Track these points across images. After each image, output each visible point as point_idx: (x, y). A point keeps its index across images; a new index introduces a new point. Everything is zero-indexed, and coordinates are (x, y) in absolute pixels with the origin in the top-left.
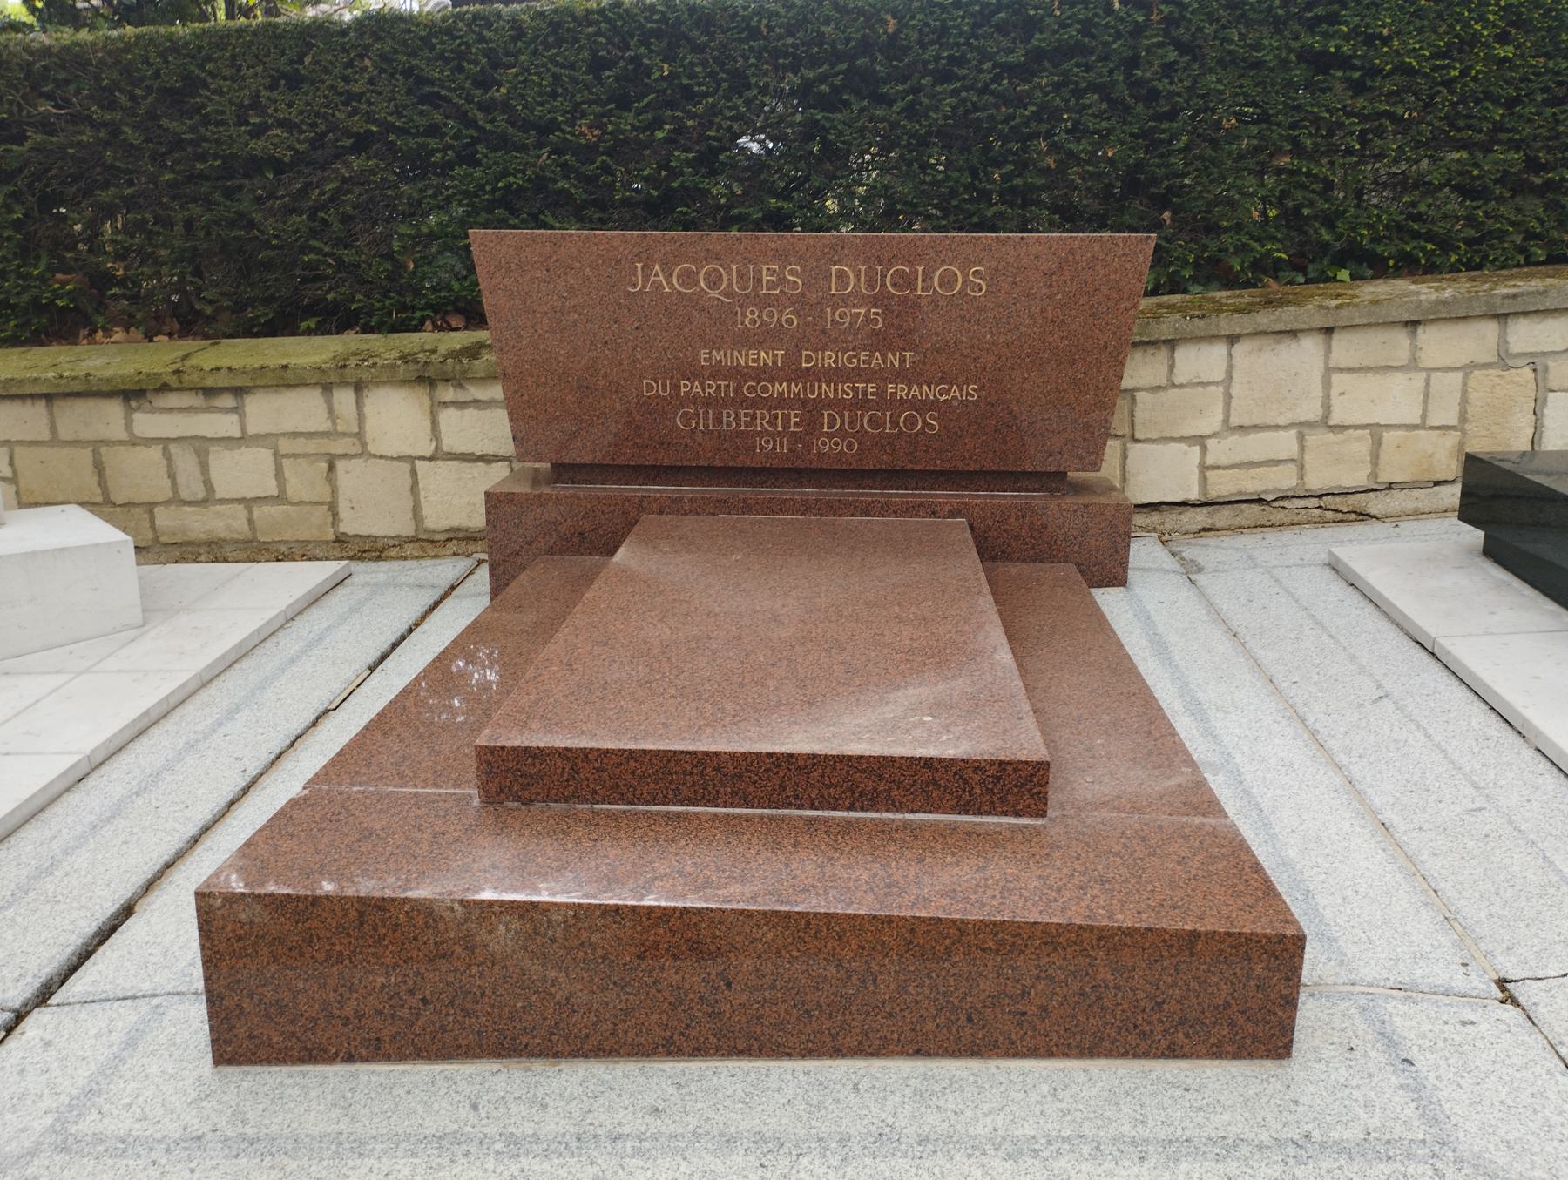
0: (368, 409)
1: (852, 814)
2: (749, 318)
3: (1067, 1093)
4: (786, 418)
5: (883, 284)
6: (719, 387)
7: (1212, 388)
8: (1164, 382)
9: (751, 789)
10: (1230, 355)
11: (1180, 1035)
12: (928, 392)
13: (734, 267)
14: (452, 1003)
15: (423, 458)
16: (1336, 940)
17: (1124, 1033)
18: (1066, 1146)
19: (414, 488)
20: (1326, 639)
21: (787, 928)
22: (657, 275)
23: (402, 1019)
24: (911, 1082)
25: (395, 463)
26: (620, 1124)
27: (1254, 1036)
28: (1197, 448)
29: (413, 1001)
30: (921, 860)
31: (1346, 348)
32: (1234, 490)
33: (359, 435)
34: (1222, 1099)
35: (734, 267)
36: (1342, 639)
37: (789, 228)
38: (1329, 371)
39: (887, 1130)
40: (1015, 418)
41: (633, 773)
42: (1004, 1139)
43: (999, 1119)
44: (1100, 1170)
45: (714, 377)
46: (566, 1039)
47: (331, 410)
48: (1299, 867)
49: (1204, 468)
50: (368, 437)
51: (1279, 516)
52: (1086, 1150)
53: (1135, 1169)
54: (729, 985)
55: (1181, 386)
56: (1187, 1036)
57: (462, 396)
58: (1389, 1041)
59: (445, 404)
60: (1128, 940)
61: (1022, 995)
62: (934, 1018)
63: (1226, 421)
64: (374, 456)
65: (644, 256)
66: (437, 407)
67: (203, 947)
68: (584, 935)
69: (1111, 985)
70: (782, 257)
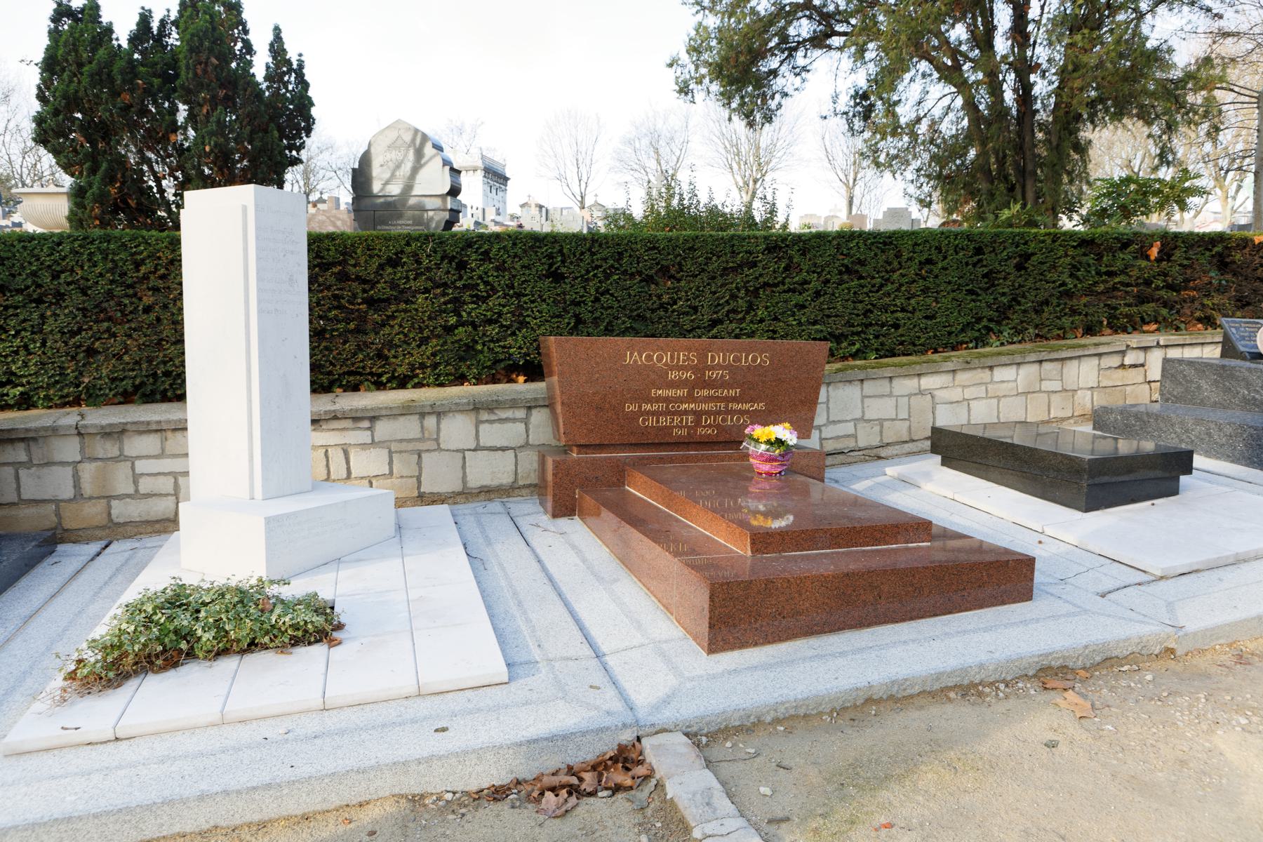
0: (442, 426)
2: (672, 375)
12: (746, 406)
19: (464, 467)
31: (869, 387)
33: (437, 440)
37: (35, 406)
38: (864, 397)
45: (657, 402)
47: (422, 427)
50: (441, 440)
51: (850, 460)
57: (493, 417)
59: (482, 422)
66: (478, 423)
70: (689, 350)
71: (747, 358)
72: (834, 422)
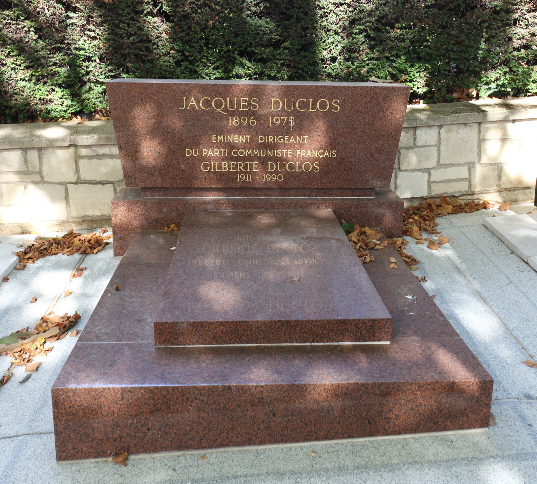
1: (313, 344)
3: (408, 447)
4: (251, 165)
5: (295, 106)
6: (221, 152)
7: (432, 148)
8: (412, 145)
9: (271, 336)
10: (439, 133)
11: (449, 422)
13: (228, 99)
14: (160, 429)
15: (72, 183)
16: (501, 383)
17: (427, 423)
18: (411, 466)
20: (485, 258)
21: (298, 391)
22: (192, 102)
23: (139, 437)
24: (348, 448)
25: (57, 186)
26: (236, 472)
27: (475, 420)
28: (427, 174)
29: (144, 429)
30: (346, 361)
32: (442, 192)
33: (40, 173)
34: (465, 444)
35: (228, 99)
36: (492, 258)
39: (342, 466)
40: (353, 165)
41: (222, 331)
42: (387, 465)
43: (384, 458)
44: (424, 473)
46: (207, 441)
48: (485, 355)
49: (430, 183)
50: (44, 174)
52: (418, 466)
53: (437, 472)
54: (274, 415)
55: (419, 147)
56: (451, 422)
58: (523, 419)
60: (429, 387)
61: (390, 411)
62: (356, 423)
63: (438, 162)
64: (47, 182)
65: (187, 94)
67: (54, 412)
68: (216, 398)
69: (423, 404)
71: (314, 104)
72: (446, 166)
